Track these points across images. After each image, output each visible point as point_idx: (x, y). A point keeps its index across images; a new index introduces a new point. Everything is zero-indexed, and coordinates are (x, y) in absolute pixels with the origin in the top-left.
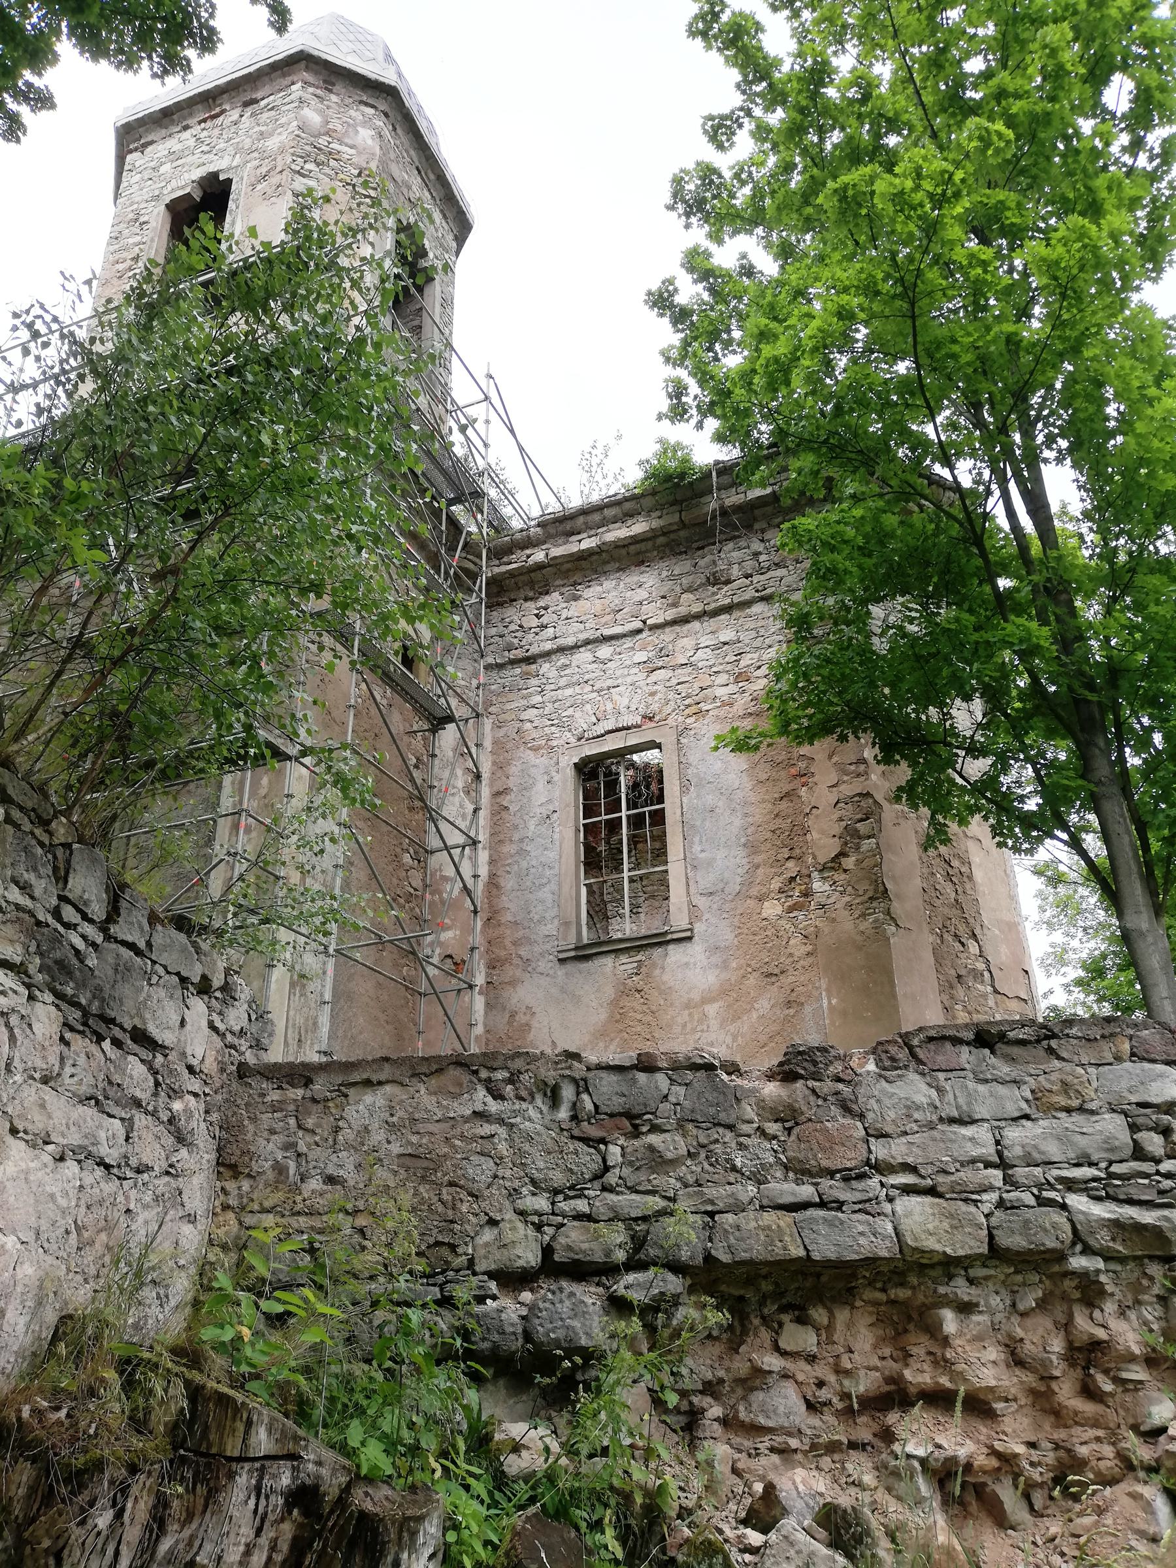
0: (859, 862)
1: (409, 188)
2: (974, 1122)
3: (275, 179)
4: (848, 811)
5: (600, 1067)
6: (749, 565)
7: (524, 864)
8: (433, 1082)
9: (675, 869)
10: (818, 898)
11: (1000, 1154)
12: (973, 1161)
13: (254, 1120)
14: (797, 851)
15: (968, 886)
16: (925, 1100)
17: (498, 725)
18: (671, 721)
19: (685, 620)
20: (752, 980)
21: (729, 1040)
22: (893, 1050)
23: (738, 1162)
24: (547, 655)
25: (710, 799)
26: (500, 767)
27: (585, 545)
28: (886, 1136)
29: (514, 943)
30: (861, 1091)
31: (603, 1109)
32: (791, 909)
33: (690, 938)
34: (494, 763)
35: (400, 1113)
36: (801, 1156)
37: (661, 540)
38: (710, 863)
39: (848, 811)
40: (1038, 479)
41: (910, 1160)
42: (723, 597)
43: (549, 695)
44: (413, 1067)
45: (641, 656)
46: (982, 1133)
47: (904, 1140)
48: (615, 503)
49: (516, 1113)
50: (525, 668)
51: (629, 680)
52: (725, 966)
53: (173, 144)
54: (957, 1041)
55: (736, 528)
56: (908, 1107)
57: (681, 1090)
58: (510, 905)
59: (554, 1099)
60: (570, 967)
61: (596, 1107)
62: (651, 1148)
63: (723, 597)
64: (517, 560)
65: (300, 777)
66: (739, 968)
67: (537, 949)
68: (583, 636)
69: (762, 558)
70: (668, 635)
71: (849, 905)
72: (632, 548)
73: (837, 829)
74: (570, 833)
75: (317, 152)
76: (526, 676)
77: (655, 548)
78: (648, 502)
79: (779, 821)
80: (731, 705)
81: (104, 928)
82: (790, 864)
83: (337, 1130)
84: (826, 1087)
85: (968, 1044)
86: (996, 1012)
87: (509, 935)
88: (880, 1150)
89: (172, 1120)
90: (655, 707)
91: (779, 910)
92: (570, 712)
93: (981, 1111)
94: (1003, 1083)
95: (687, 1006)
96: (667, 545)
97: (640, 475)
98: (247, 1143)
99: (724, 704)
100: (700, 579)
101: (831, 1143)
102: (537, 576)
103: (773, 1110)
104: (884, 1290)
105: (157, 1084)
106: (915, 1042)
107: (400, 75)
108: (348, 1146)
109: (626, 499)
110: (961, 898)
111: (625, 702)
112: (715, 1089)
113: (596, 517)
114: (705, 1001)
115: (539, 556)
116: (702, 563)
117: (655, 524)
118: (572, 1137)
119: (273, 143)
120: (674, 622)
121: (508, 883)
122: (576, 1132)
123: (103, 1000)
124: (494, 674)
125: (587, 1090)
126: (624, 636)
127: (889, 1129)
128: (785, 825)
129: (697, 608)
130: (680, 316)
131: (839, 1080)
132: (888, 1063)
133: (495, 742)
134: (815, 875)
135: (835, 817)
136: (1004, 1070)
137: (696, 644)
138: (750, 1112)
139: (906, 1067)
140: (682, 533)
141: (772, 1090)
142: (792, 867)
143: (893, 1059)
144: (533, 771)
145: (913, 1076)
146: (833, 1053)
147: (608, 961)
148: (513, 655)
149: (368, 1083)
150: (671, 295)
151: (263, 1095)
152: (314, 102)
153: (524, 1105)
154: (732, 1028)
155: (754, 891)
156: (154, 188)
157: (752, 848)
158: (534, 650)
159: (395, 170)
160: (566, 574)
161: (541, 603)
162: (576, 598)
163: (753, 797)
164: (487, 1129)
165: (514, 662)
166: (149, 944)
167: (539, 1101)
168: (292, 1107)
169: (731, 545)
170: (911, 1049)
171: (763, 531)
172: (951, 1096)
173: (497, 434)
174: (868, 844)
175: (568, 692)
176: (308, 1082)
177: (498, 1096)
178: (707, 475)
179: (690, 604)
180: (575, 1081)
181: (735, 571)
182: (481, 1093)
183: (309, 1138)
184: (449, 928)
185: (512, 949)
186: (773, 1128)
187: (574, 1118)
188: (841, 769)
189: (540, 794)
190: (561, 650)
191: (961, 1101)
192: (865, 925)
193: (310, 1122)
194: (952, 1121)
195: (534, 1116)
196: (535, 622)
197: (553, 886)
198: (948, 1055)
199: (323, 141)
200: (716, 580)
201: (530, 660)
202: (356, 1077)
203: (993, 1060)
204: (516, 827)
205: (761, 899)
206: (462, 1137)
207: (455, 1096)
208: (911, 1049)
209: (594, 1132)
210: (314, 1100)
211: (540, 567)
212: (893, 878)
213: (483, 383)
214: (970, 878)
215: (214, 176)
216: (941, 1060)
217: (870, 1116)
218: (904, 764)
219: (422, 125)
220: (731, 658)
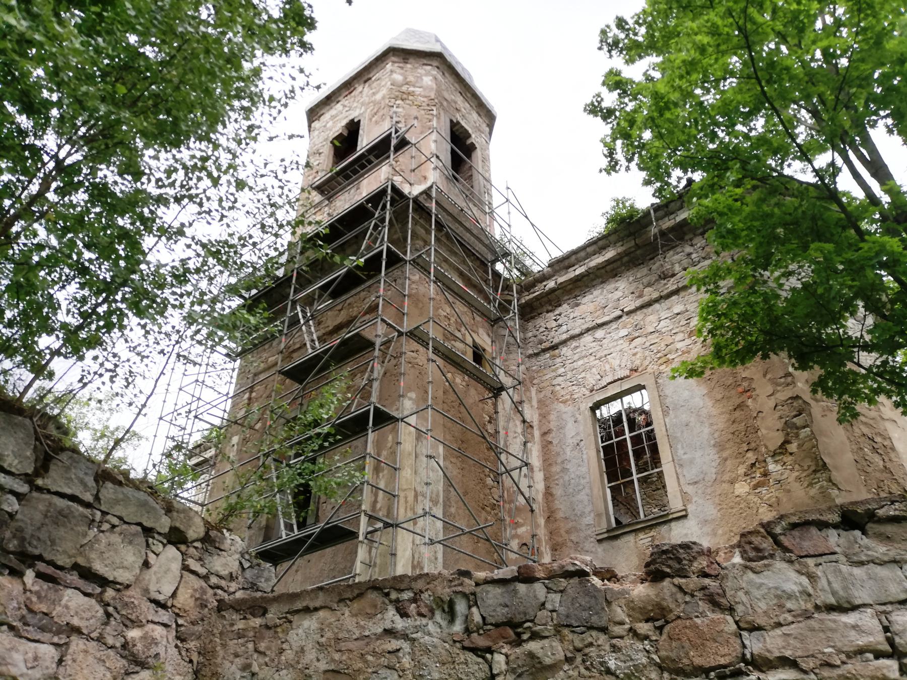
0: (800, 446)
1: (456, 103)
2: (854, 608)
3: (381, 113)
4: (786, 410)
5: (487, 582)
6: (685, 263)
7: (567, 478)
8: (356, 605)
9: (667, 467)
10: (774, 476)
11: (891, 642)
12: (861, 651)
13: (224, 646)
14: (753, 445)
15: (892, 455)
16: (796, 588)
17: (540, 391)
18: (649, 370)
22: (757, 540)
23: (612, 664)
24: (564, 342)
25: (684, 417)
26: (544, 416)
27: (578, 272)
28: (759, 628)
29: (567, 532)
30: (729, 584)
31: (490, 620)
32: (756, 487)
33: (685, 516)
34: (540, 415)
35: (329, 634)
36: (673, 655)
37: (626, 259)
38: (692, 461)
39: (786, 410)
40: (873, 150)
41: (788, 653)
42: (671, 285)
43: (568, 366)
44: (340, 594)
45: (624, 332)
46: (867, 619)
47: (778, 631)
48: (592, 243)
49: (417, 629)
50: (552, 353)
51: (618, 348)
53: (333, 112)
54: (822, 525)
55: (672, 241)
56: (778, 597)
57: (557, 597)
58: (562, 507)
59: (451, 615)
60: (605, 545)
61: (484, 618)
62: (531, 655)
63: (671, 285)
64: (538, 290)
65: (410, 433)
66: (724, 534)
67: (582, 535)
68: (585, 327)
69: (694, 256)
70: (639, 316)
71: (798, 479)
72: (608, 268)
73: (780, 424)
74: (593, 453)
75: (402, 95)
76: (553, 357)
77: (623, 265)
78: (613, 238)
79: (735, 425)
80: (688, 352)
81: (28, 479)
82: (750, 454)
83: (282, 651)
84: (693, 582)
85: (835, 526)
86: (854, 491)
87: (563, 527)
88: (754, 645)
89: (124, 646)
90: (638, 362)
91: (747, 488)
92: (583, 375)
93: (861, 596)
94: (882, 563)
96: (629, 262)
97: (604, 221)
98: (216, 665)
100: (654, 278)
101: (702, 640)
102: (553, 296)
103: (642, 610)
105: (108, 615)
106: (778, 530)
107: (442, 44)
108: (289, 666)
109: (599, 239)
110: (888, 465)
111: (618, 362)
112: (587, 593)
113: (583, 254)
115: (551, 284)
116: (654, 267)
117: (620, 250)
118: (464, 648)
119: (378, 97)
121: (558, 491)
122: (467, 644)
123: (23, 539)
124: (533, 360)
125: (476, 604)
126: (611, 321)
127: (761, 621)
128: (742, 427)
129: (655, 295)
130: (607, 114)
131: (706, 575)
132: (752, 554)
133: (539, 401)
134: (769, 460)
136: (880, 550)
137: (659, 318)
138: (620, 613)
139: (772, 556)
140: (638, 252)
141: (641, 591)
142: (751, 457)
143: (757, 549)
144: (564, 416)
145: (779, 565)
146: (696, 548)
147: (630, 538)
148: (543, 346)
149: (307, 610)
150: (599, 103)
151: (232, 625)
152: (398, 70)
153: (424, 621)
155: (727, 477)
156: (324, 135)
157: (720, 446)
158: (556, 341)
159: (446, 95)
160: (569, 292)
161: (557, 312)
162: (578, 305)
163: (714, 412)
164: (394, 644)
165: (544, 351)
166: (97, 498)
167: (438, 616)
168: (251, 634)
169: (671, 253)
170: (775, 538)
171: (691, 240)
172: (823, 582)
173: (517, 220)
175: (581, 362)
176: (265, 612)
177: (404, 614)
178: (647, 213)
179: (650, 293)
180: (465, 595)
181: (677, 268)
182: (391, 612)
183: (262, 660)
184: (522, 525)
185: (566, 536)
186: (644, 628)
187: (467, 631)
188: (773, 382)
189: (571, 430)
190: (573, 338)
191: (836, 586)
192: (813, 491)
193: (262, 646)
194: (830, 608)
195: (433, 631)
196: (554, 324)
197: (587, 490)
198: (814, 540)
199: (404, 88)
200: (665, 276)
201: (554, 347)
202: (299, 605)
203: (865, 541)
204: (558, 454)
205: (732, 482)
206: (374, 653)
207: (370, 616)
208: (775, 538)
209: (480, 641)
210: (268, 627)
211: (553, 291)
212: (829, 454)
213: (504, 192)
214: (893, 449)
215: (352, 120)
216: (808, 546)
217: (740, 609)
218: (816, 367)
219: (449, 58)
220: (683, 322)
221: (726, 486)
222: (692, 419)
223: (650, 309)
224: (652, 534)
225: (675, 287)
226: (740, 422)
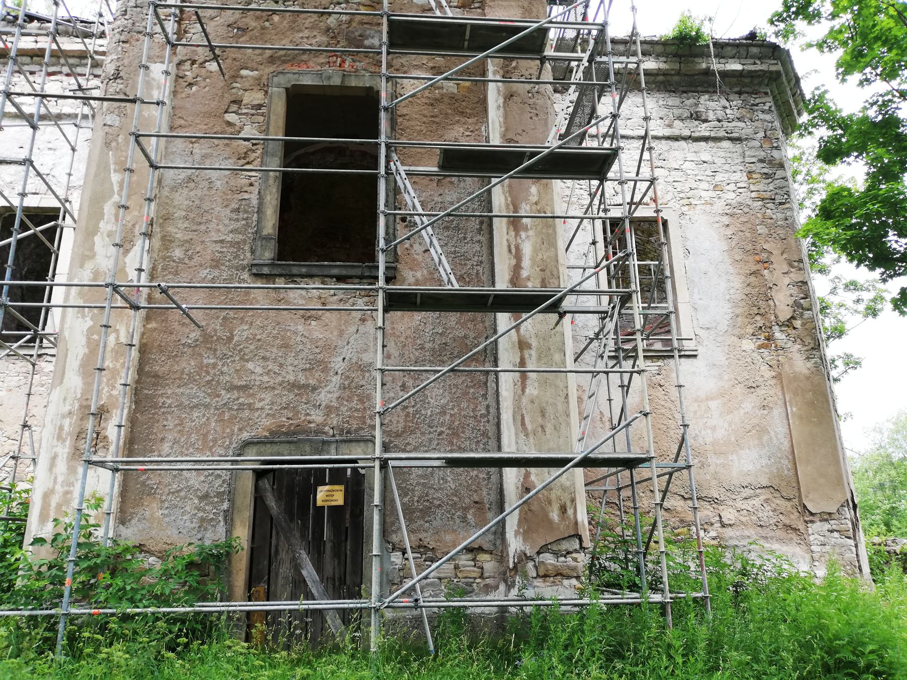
0: (803, 325)
19: (676, 138)
20: (739, 389)
21: (726, 425)
32: (760, 347)
33: (695, 356)
37: (661, 78)
42: (703, 130)
52: (720, 378)
63: (703, 130)
69: (728, 111)
73: (790, 301)
95: (696, 401)
96: (662, 82)
99: (706, 203)
100: (687, 114)
104: (77, 480)
114: (708, 399)
117: (663, 66)
120: (668, 138)
129: (686, 133)
135: (788, 293)
140: (676, 78)
154: (729, 418)
169: (707, 97)
174: (807, 314)
179: (681, 128)
200: (696, 117)
220: (709, 173)
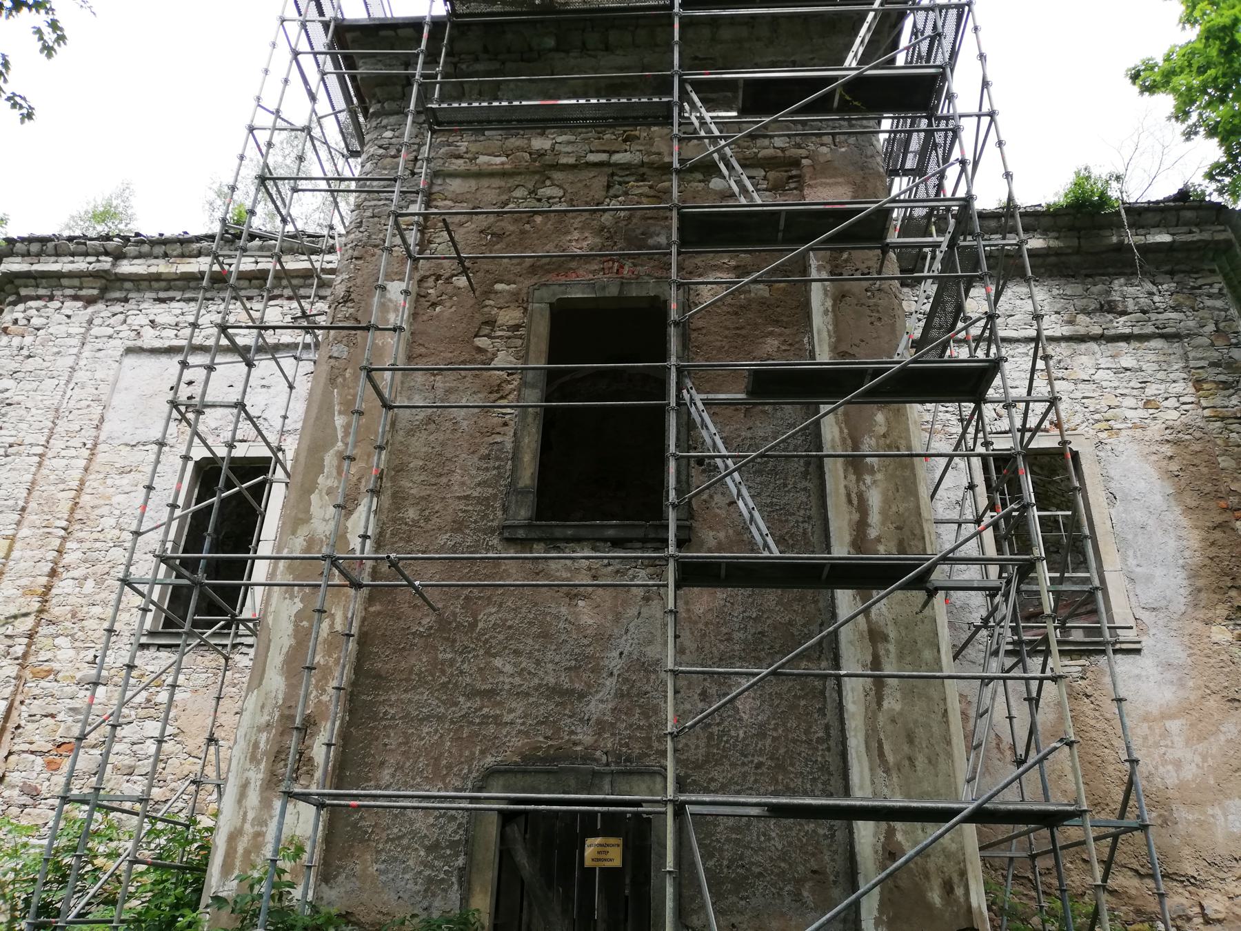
25: (1139, 516)
33: (1138, 651)
37: (1052, 259)
42: (1121, 325)
63: (1121, 325)
69: (1156, 299)
116: (1095, 289)
117: (1054, 243)
129: (1097, 330)
157: (1193, 575)
163: (1185, 522)
169: (1122, 280)
179: (1085, 324)
221: (1199, 625)
222: (1150, 522)
223: (1083, 346)
224: (1082, 662)
225: (1128, 331)
226: (1222, 547)
